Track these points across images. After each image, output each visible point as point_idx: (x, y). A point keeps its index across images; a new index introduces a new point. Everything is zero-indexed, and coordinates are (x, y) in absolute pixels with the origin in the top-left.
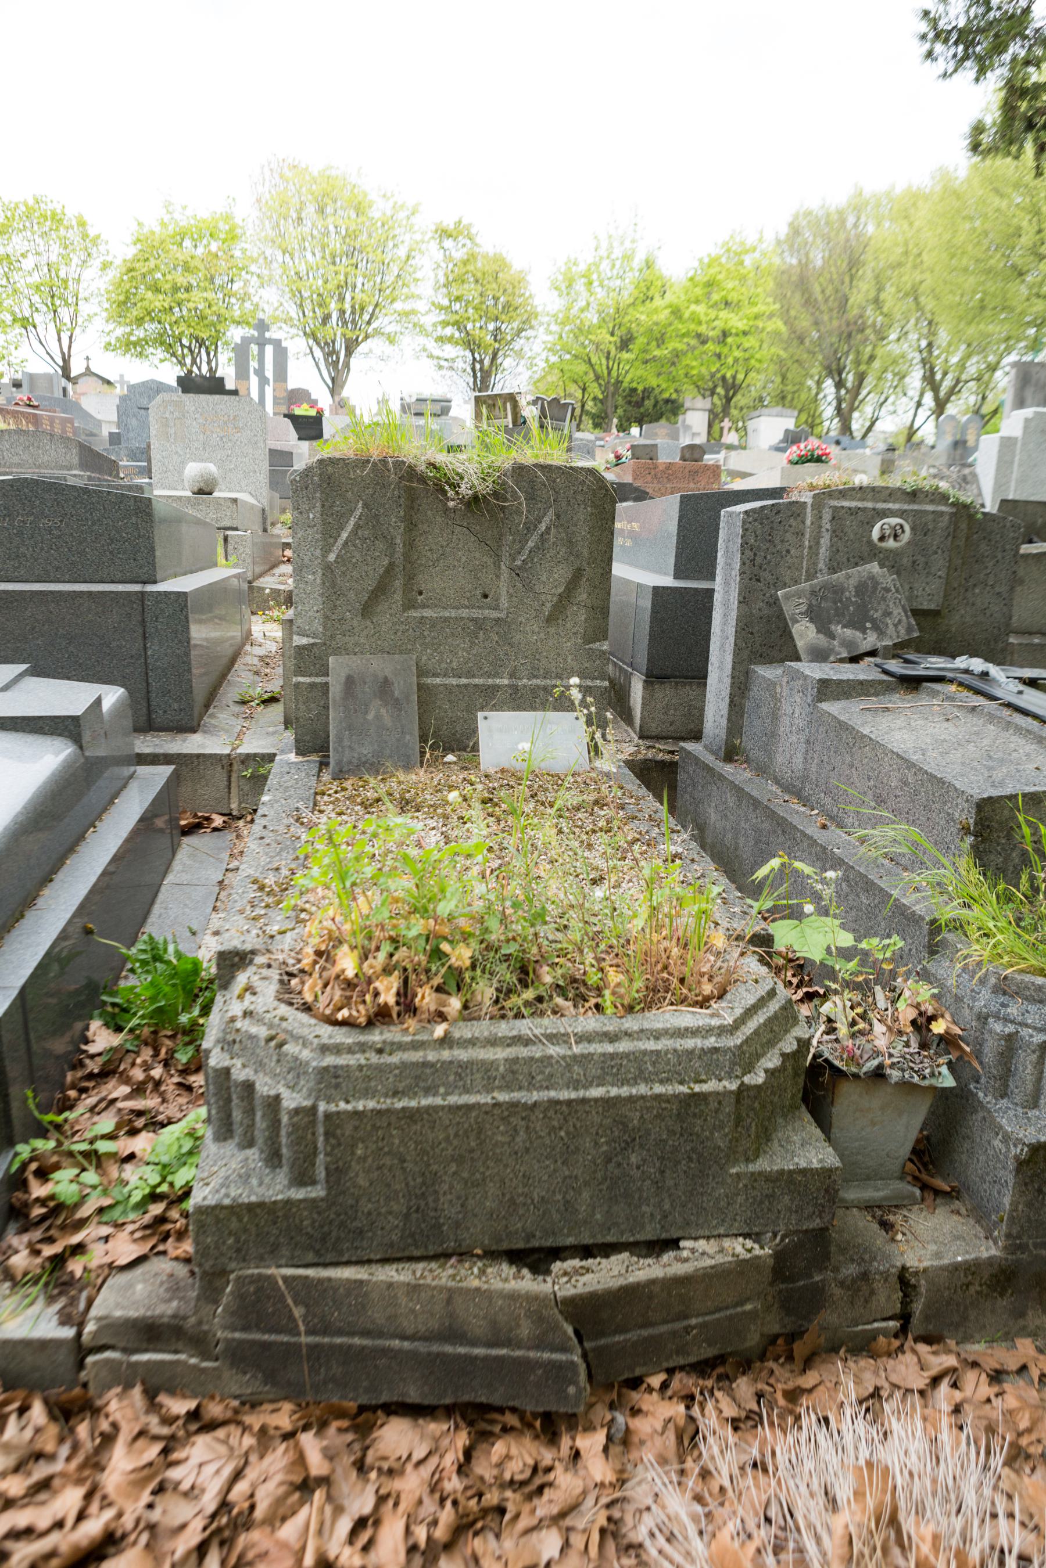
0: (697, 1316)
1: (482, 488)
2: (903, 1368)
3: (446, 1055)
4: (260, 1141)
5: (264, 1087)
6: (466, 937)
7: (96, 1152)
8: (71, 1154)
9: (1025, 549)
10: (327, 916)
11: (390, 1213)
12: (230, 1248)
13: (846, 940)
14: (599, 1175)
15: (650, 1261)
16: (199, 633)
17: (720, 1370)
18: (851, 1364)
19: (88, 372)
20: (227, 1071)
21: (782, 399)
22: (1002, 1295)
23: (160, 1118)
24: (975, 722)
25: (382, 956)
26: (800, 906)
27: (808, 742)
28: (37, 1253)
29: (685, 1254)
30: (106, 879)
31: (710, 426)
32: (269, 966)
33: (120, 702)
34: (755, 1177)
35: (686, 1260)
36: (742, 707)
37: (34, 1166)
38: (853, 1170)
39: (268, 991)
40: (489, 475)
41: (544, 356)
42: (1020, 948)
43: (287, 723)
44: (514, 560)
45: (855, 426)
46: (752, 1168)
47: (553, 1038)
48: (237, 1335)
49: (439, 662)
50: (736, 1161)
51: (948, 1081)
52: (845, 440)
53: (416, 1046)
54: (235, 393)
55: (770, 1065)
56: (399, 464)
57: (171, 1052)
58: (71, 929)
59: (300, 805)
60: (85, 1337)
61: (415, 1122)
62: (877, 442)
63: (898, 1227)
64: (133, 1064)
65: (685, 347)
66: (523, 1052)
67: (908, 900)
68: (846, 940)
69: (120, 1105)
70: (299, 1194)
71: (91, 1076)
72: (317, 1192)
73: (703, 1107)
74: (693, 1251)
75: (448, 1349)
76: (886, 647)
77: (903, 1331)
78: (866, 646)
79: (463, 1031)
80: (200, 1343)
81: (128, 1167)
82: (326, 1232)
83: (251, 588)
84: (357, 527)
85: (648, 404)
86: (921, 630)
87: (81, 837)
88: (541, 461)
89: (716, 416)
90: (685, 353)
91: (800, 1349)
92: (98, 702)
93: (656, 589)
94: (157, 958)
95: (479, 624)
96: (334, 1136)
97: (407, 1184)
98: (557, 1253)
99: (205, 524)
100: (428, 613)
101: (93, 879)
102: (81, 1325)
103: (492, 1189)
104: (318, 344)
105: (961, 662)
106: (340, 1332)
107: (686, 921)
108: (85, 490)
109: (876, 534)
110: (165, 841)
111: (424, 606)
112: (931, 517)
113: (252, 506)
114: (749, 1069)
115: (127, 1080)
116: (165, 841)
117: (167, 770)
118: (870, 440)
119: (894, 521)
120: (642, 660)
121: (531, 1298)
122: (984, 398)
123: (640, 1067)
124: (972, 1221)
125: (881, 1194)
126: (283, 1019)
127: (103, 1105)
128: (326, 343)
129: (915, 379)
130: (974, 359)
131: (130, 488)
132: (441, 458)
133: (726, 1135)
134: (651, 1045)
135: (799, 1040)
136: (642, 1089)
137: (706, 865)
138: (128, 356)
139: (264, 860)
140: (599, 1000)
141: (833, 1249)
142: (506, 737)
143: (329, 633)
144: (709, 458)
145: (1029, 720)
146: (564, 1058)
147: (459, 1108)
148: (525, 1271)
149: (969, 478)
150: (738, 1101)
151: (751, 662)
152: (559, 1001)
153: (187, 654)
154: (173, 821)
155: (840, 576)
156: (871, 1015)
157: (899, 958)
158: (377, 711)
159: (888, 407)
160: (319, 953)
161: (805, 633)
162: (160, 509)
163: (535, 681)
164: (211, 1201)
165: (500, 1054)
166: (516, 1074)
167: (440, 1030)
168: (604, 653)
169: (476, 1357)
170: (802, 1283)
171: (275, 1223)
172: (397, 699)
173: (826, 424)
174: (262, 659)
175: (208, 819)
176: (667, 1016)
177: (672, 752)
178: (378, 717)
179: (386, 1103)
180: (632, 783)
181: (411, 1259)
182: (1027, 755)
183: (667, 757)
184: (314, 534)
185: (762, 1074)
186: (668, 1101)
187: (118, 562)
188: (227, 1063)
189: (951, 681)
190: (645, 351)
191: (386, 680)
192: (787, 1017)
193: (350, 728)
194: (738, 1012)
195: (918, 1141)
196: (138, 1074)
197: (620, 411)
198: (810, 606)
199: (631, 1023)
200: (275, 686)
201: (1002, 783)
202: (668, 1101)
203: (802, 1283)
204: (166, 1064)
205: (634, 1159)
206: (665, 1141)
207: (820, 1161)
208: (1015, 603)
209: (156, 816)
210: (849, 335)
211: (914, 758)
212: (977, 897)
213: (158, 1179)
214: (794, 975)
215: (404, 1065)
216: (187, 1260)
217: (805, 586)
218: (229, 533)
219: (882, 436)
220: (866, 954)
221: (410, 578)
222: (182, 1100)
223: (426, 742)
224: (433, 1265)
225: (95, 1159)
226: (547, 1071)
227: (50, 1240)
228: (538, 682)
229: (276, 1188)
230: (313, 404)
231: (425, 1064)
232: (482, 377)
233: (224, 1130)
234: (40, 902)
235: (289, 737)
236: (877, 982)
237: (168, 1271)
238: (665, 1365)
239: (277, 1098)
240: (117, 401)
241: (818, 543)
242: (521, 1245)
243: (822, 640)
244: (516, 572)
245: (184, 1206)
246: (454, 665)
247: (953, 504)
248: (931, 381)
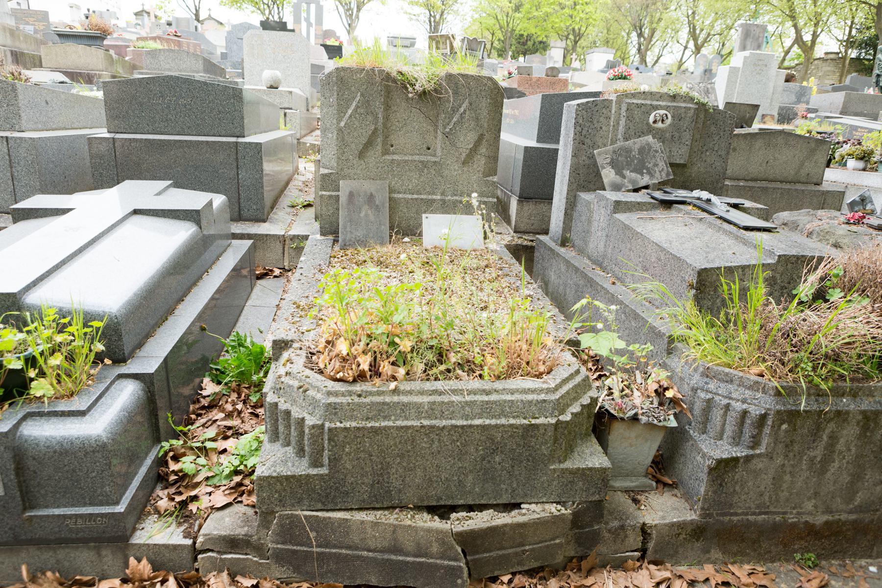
1: (429, 87)
2: (641, 577)
3: (396, 399)
4: (293, 443)
5: (296, 413)
6: (408, 335)
7: (205, 447)
8: (192, 448)
9: (737, 131)
10: (334, 321)
11: (363, 483)
12: (276, 499)
13: (621, 345)
14: (478, 467)
15: (504, 514)
16: (269, 167)
17: (541, 574)
18: (612, 574)
19: (210, 18)
20: (276, 404)
21: (607, 42)
22: (697, 541)
23: (241, 431)
24: (701, 227)
25: (362, 344)
26: (595, 326)
27: (607, 236)
28: (173, 499)
29: (524, 511)
30: (214, 302)
31: (564, 57)
32: (301, 349)
33: (223, 203)
34: (563, 471)
35: (524, 515)
36: (572, 216)
37: (171, 454)
38: (618, 470)
39: (300, 361)
40: (432, 79)
41: (471, 13)
42: (717, 352)
43: (316, 218)
44: (445, 128)
45: (648, 60)
46: (562, 466)
47: (454, 392)
48: (279, 546)
50: (554, 462)
51: (673, 423)
52: (642, 67)
53: (380, 393)
54: (293, 31)
55: (575, 411)
56: (381, 72)
57: (247, 396)
58: (193, 328)
59: (322, 262)
61: (378, 435)
62: (661, 69)
63: (642, 502)
64: (227, 402)
65: (552, 11)
66: (438, 399)
67: (657, 323)
68: (621, 345)
69: (218, 423)
70: (314, 471)
71: (203, 408)
72: (324, 471)
74: (528, 510)
75: (393, 557)
76: (654, 184)
77: (642, 558)
78: (643, 183)
79: (406, 386)
80: (259, 550)
81: (222, 456)
82: (329, 493)
83: (299, 143)
84: (357, 107)
85: (530, 43)
86: (675, 174)
87: (200, 277)
88: (462, 72)
89: (568, 51)
90: (551, 14)
91: (585, 565)
92: (210, 203)
93: (526, 148)
94: (240, 345)
95: (424, 164)
96: (334, 441)
98: (454, 508)
99: (273, 105)
100: (396, 157)
101: (206, 300)
102: (195, 539)
103: (419, 472)
104: (341, 4)
105: (696, 193)
106: (335, 547)
107: (532, 333)
108: (205, 83)
109: (651, 119)
110: (247, 282)
111: (394, 153)
112: (683, 110)
113: (301, 96)
114: (562, 412)
115: (223, 411)
116: (247, 282)
117: (249, 243)
118: (656, 68)
119: (662, 112)
120: (517, 189)
121: (439, 532)
122: (723, 45)
123: (502, 409)
124: (683, 501)
125: (634, 484)
126: (307, 377)
127: (210, 423)
128: (346, 4)
129: (684, 34)
130: (719, 22)
131: (231, 83)
132: (405, 69)
134: (509, 397)
135: (591, 398)
136: (503, 421)
137: (547, 302)
138: (233, 8)
139: (300, 292)
140: (481, 372)
141: (605, 512)
142: (436, 228)
144: (562, 76)
145: (732, 226)
146: (460, 402)
147: (402, 427)
148: (436, 517)
149: (710, 90)
150: (556, 430)
151: (578, 190)
152: (459, 372)
153: (261, 178)
154: (252, 271)
155: (630, 143)
156: (632, 386)
157: (650, 356)
158: (366, 212)
159: (668, 49)
160: (328, 342)
161: (608, 175)
162: (247, 96)
163: (455, 198)
164: (266, 474)
165: (426, 399)
166: (433, 410)
167: (393, 385)
168: (494, 182)
169: (408, 562)
173: (632, 58)
174: (304, 182)
175: (272, 271)
176: (519, 382)
177: (532, 241)
178: (366, 215)
179: (362, 424)
180: (508, 256)
181: (374, 509)
182: (729, 246)
183: (529, 244)
184: (333, 111)
185: (570, 415)
186: (517, 428)
187: (223, 125)
188: (276, 400)
189: (689, 204)
190: (529, 13)
191: (371, 195)
192: (585, 385)
194: (558, 381)
195: (655, 456)
196: (229, 407)
197: (513, 48)
198: (612, 159)
199: (499, 385)
200: (311, 198)
201: (713, 261)
202: (517, 428)
204: (245, 402)
205: (497, 459)
207: (600, 464)
208: (729, 161)
209: (242, 268)
210: (647, 6)
211: (665, 246)
212: (695, 323)
213: (238, 463)
214: (593, 365)
215: (373, 404)
216: (253, 506)
217: (610, 148)
218: (287, 111)
219: (664, 66)
220: (632, 353)
221: (387, 137)
222: (253, 422)
223: (393, 230)
224: (386, 512)
225: (203, 451)
226: (451, 409)
227: (180, 493)
228: (457, 198)
229: (302, 468)
230: (337, 38)
231: (384, 403)
232: (434, 25)
233: (275, 437)
234: (176, 312)
235: (317, 225)
236: (637, 368)
237: (243, 511)
238: (511, 570)
239: (303, 419)
240: (226, 34)
241: (618, 124)
242: (434, 504)
243: (618, 179)
244: (446, 135)
245: (252, 477)
246: (410, 187)
247: (696, 103)
248: (693, 35)
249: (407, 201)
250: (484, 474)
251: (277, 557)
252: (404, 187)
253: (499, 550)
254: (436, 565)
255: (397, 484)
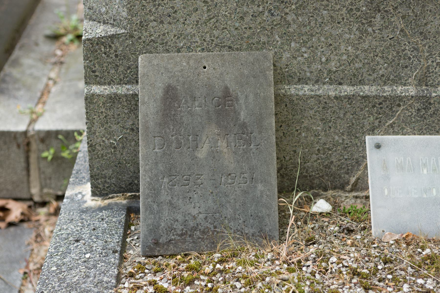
49: (309, 62)
143: (137, 20)
158: (212, 145)
172: (244, 126)
178: (214, 154)
191: (227, 94)
193: (170, 172)
246: (333, 65)
249: (323, 103)
252: (316, 66)
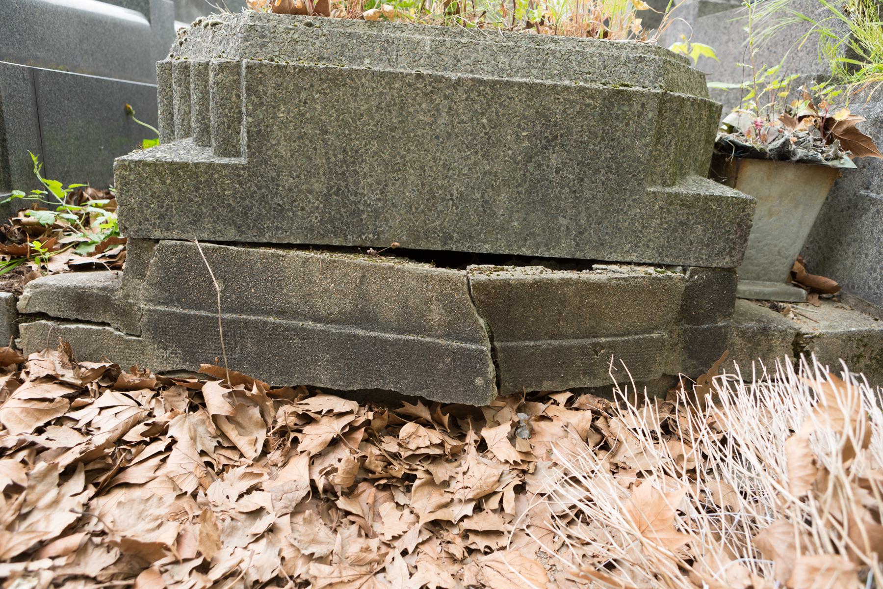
0: (607, 336)
11: (310, 192)
14: (519, 175)
34: (672, 198)
48: (159, 308)
50: (654, 183)
60: (21, 305)
73: (626, 108)
97: (328, 159)
106: (256, 311)
133: (646, 145)
169: (386, 341)
170: (706, 326)
171: (197, 189)
186: (591, 97)
203: (706, 326)
206: (587, 143)
226: (473, 56)
238: (572, 384)
250: (529, 192)
251: (156, 328)
253: (551, 338)
254: (437, 347)
255: (372, 198)
